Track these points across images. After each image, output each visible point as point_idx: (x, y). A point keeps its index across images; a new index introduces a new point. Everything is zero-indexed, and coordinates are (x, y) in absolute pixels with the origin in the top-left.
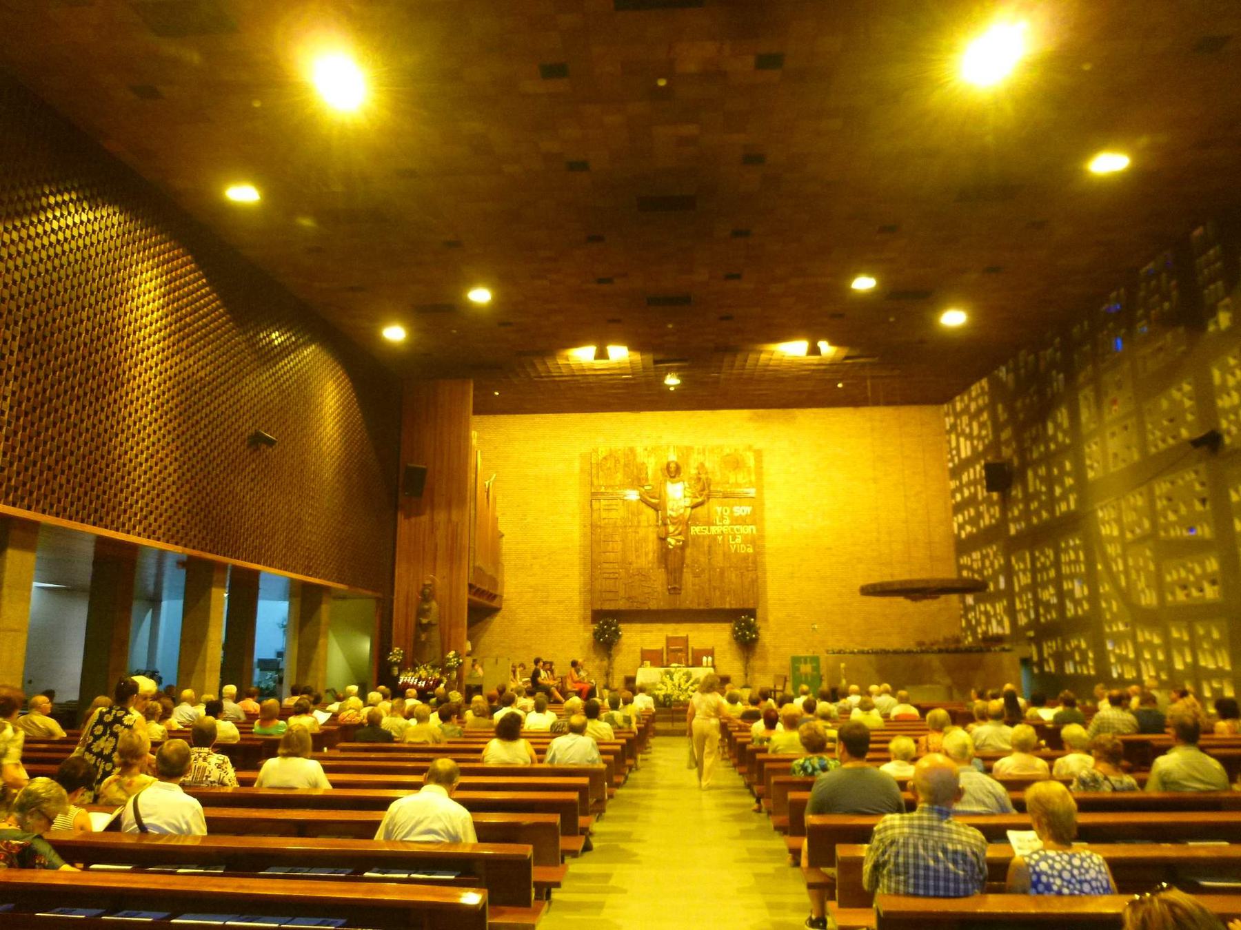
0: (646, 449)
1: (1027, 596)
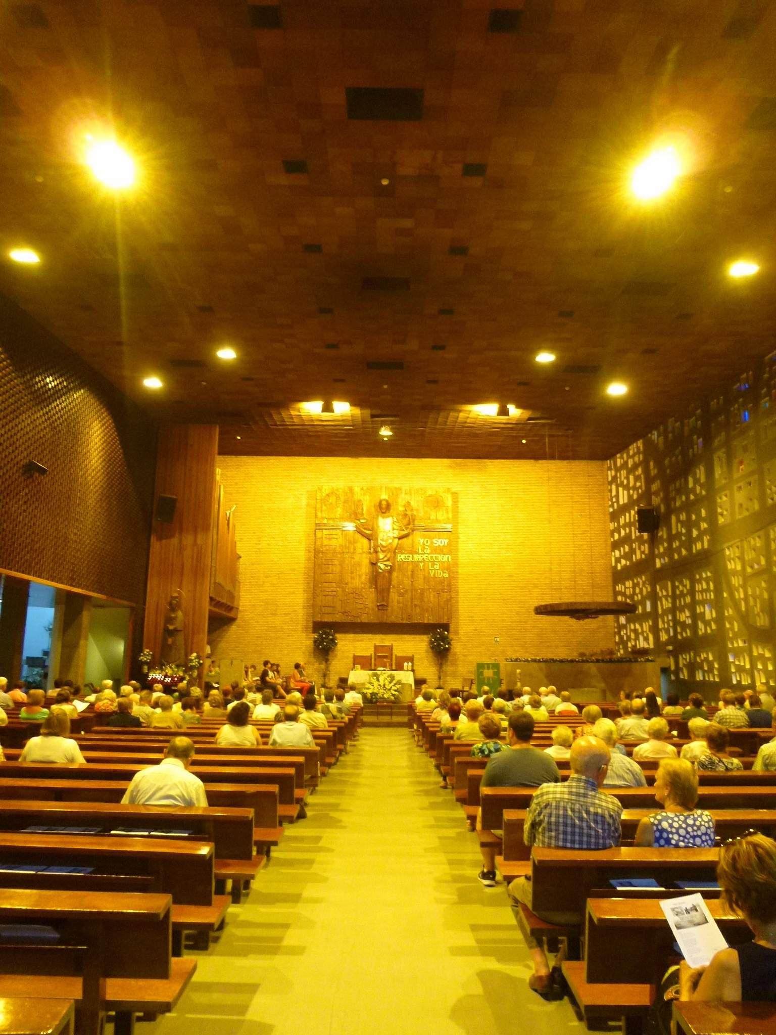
1: (668, 617)
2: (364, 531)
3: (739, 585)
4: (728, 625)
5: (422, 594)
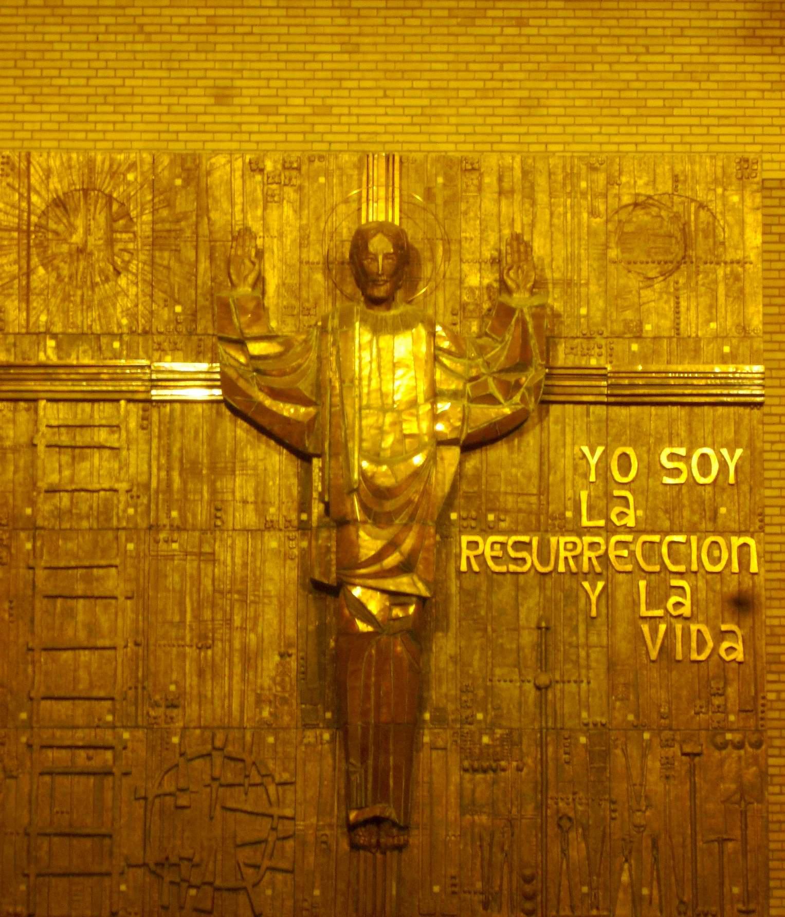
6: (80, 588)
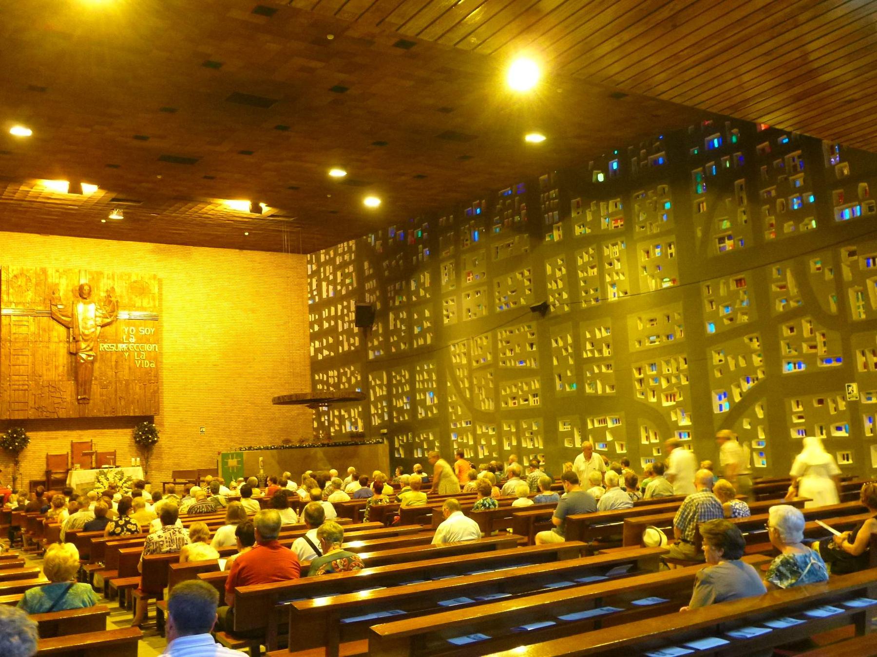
0: (57, 271)
1: (382, 404)
2: (63, 318)
3: (464, 376)
4: (450, 410)
5: (127, 385)
6: (20, 353)
